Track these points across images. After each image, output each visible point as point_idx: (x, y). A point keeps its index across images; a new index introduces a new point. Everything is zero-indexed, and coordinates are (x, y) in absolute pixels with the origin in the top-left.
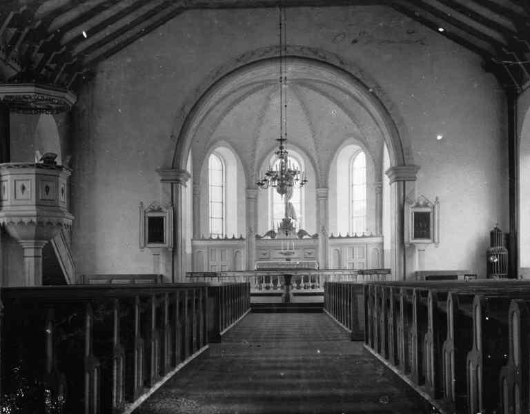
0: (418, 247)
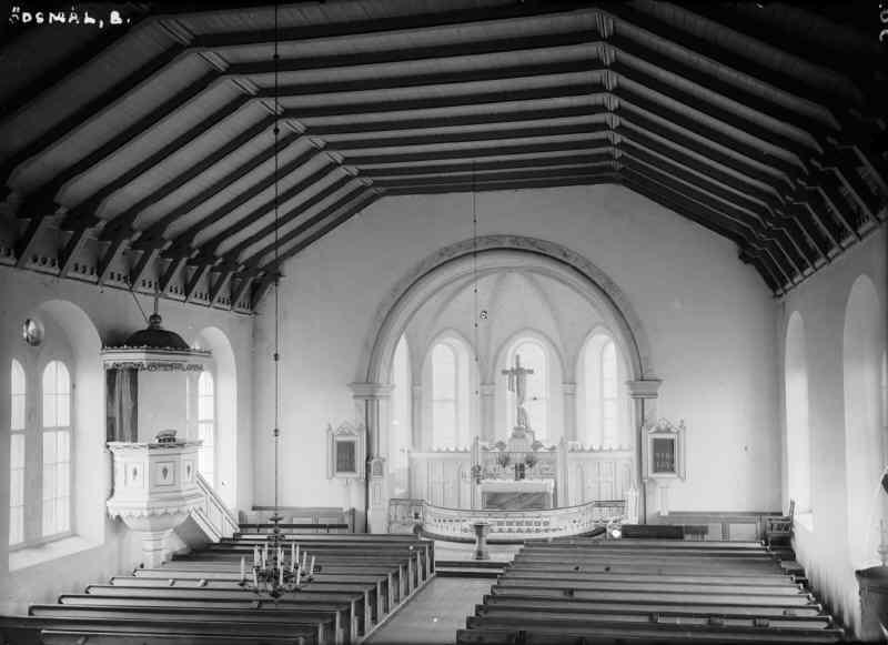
0: (662, 483)
